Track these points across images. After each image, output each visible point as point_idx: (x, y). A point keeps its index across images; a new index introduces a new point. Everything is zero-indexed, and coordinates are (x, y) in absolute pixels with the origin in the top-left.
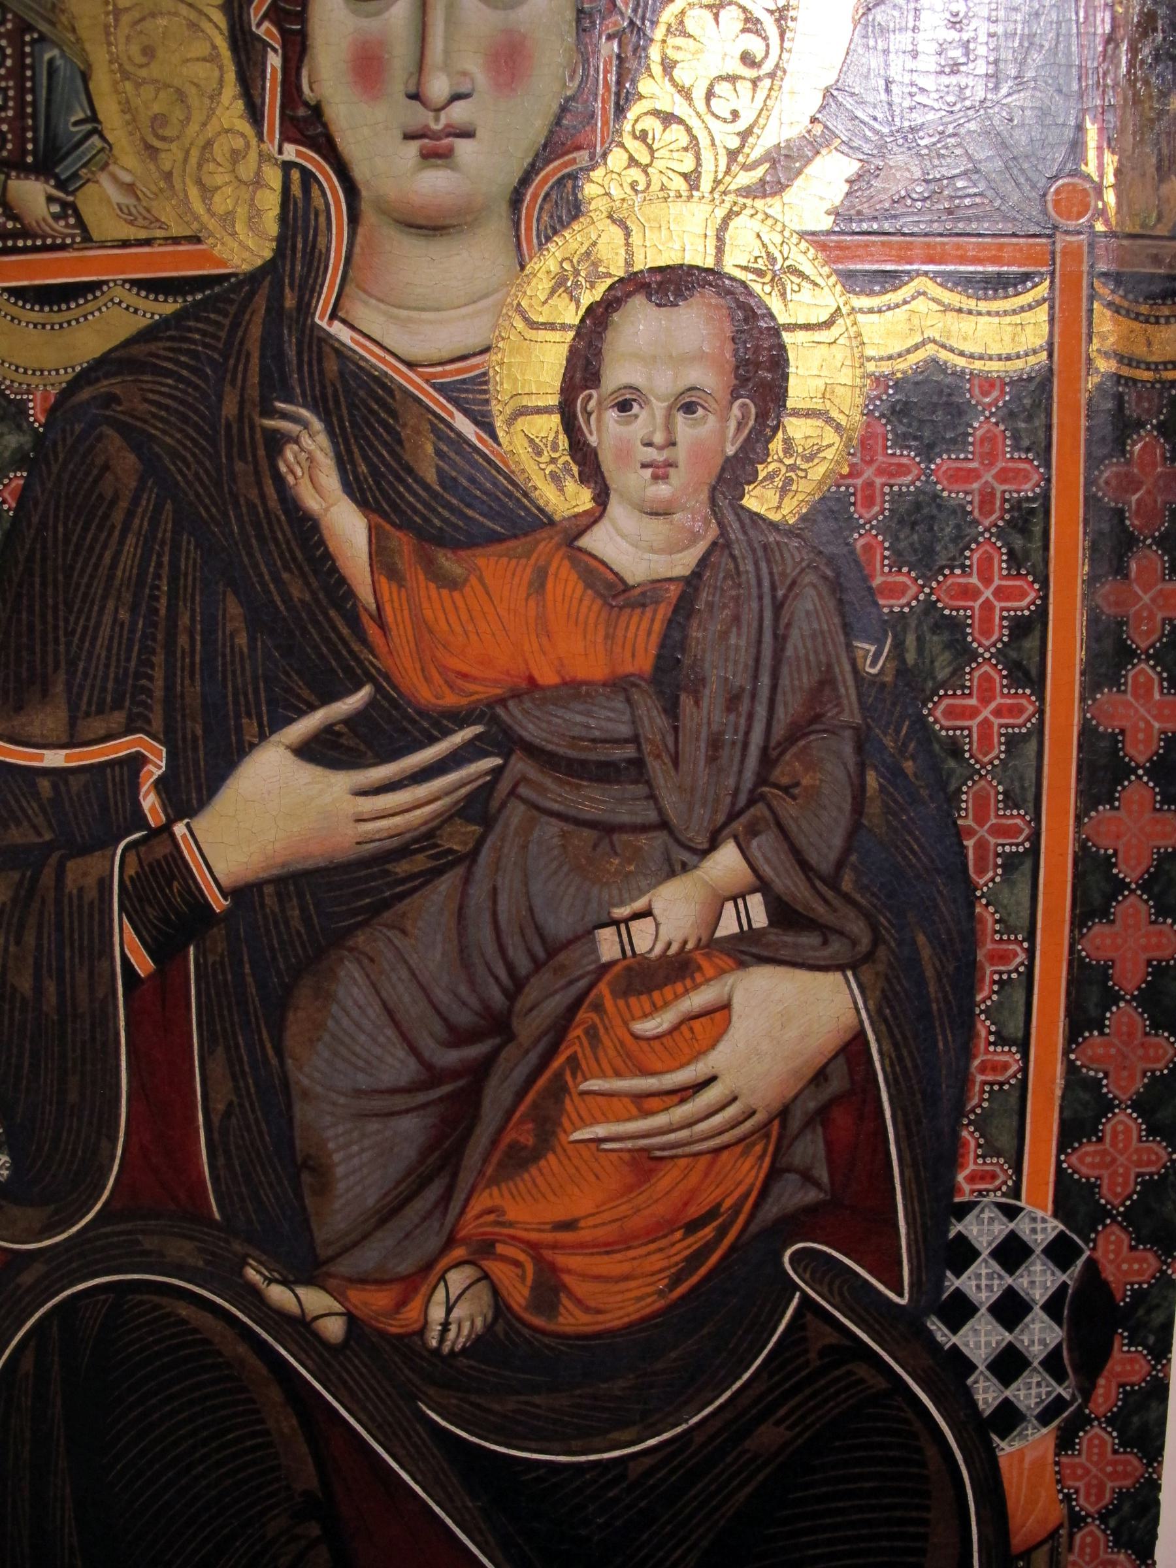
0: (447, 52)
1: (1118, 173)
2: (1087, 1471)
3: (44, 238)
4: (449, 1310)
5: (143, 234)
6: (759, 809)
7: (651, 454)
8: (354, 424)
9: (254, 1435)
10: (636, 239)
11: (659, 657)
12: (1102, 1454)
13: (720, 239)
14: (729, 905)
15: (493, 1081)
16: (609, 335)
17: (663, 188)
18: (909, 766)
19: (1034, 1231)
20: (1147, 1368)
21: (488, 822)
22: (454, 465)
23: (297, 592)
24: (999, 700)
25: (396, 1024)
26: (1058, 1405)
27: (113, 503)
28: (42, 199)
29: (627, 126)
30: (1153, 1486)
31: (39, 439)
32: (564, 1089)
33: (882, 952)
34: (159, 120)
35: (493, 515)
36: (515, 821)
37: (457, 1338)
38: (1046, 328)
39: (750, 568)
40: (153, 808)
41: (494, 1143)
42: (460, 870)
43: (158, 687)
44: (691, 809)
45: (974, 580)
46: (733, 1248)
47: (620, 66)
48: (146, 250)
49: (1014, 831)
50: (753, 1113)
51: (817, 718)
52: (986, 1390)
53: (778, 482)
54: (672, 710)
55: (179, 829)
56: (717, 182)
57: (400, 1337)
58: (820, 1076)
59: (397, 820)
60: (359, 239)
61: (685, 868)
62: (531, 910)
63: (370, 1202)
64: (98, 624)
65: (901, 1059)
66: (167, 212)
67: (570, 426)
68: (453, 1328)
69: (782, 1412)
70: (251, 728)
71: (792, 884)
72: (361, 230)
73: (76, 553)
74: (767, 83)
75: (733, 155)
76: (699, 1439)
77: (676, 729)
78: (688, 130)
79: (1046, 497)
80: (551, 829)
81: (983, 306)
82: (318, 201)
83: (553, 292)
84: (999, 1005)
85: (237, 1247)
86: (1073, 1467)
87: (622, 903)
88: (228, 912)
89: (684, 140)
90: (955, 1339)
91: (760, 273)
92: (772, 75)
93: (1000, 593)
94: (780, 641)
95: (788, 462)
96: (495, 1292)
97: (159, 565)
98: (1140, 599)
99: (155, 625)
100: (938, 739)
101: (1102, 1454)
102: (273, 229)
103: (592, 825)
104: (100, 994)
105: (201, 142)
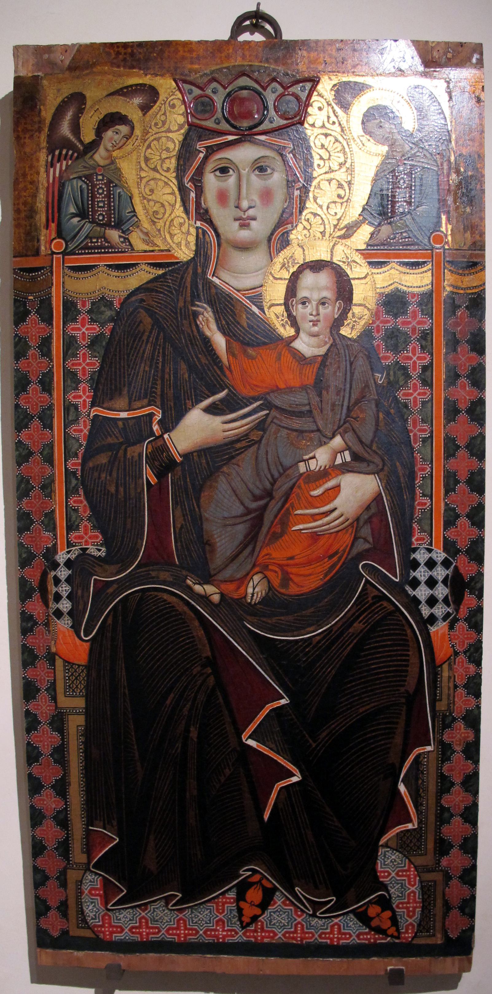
0: (247, 194)
1: (452, 230)
2: (459, 637)
3: (118, 248)
4: (254, 589)
5: (151, 249)
6: (347, 425)
7: (312, 318)
8: (220, 309)
9: (189, 638)
10: (306, 252)
11: (316, 379)
12: (463, 631)
13: (332, 252)
14: (339, 455)
15: (268, 512)
16: (299, 281)
17: (314, 236)
18: (392, 411)
19: (437, 557)
20: (475, 603)
21: (264, 430)
22: (252, 322)
23: (204, 360)
24: (419, 391)
25: (237, 495)
26: (448, 615)
27: (144, 332)
28: (117, 237)
29: (303, 217)
30: (480, 642)
31: (118, 313)
32: (290, 514)
33: (386, 468)
34: (155, 212)
35: (265, 337)
36: (273, 430)
37: (257, 599)
38: (431, 278)
39: (343, 352)
40: (157, 430)
41: (268, 532)
42: (256, 446)
43: (159, 392)
44: (326, 424)
45: (410, 354)
46: (344, 563)
47: (300, 200)
48: (153, 253)
49: (425, 431)
50: (348, 520)
51: (364, 397)
52: (425, 610)
53: (351, 326)
54: (320, 395)
55: (166, 436)
56: (331, 235)
57: (238, 599)
58: (368, 508)
59: (236, 431)
60: (221, 251)
61: (325, 443)
62: (278, 457)
63: (228, 554)
64: (138, 373)
65: (393, 501)
66: (159, 242)
67: (287, 310)
68: (255, 595)
69: (361, 618)
70: (189, 403)
71: (357, 448)
72: (221, 249)
73: (131, 349)
74: (345, 204)
75: (335, 226)
76: (335, 629)
77: (321, 401)
78: (322, 218)
79: (432, 329)
80: (284, 432)
81: (412, 271)
82: (208, 240)
83: (281, 268)
84: (422, 484)
85: (184, 573)
86: (454, 635)
87: (306, 455)
88: (182, 462)
89: (320, 222)
90: (414, 593)
91: (344, 262)
92: (347, 201)
93: (419, 358)
94: (352, 374)
95: (354, 320)
96: (269, 582)
97: (159, 353)
98: (461, 359)
99: (157, 371)
100: (401, 403)
101: (463, 631)
102: (194, 248)
103: (296, 431)
104: (139, 491)
105: (170, 219)
